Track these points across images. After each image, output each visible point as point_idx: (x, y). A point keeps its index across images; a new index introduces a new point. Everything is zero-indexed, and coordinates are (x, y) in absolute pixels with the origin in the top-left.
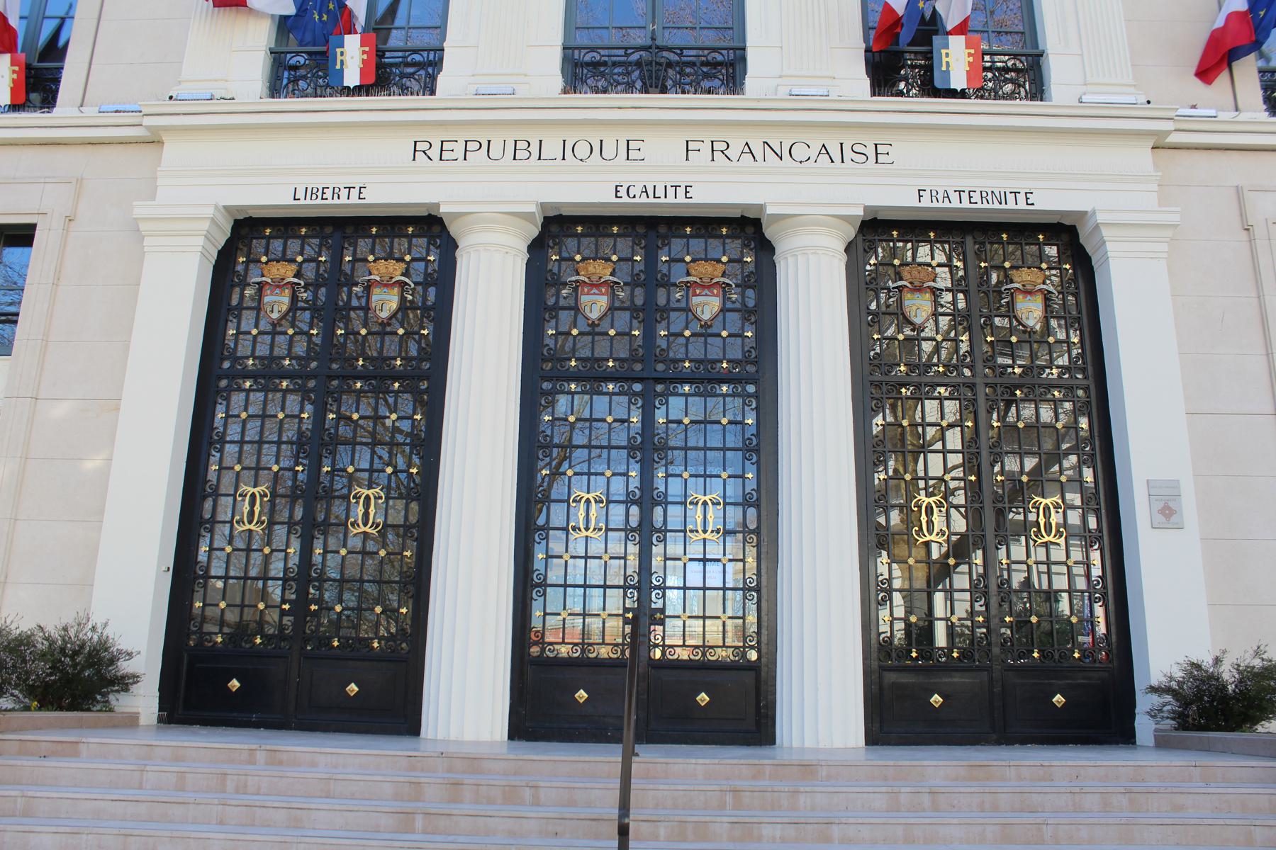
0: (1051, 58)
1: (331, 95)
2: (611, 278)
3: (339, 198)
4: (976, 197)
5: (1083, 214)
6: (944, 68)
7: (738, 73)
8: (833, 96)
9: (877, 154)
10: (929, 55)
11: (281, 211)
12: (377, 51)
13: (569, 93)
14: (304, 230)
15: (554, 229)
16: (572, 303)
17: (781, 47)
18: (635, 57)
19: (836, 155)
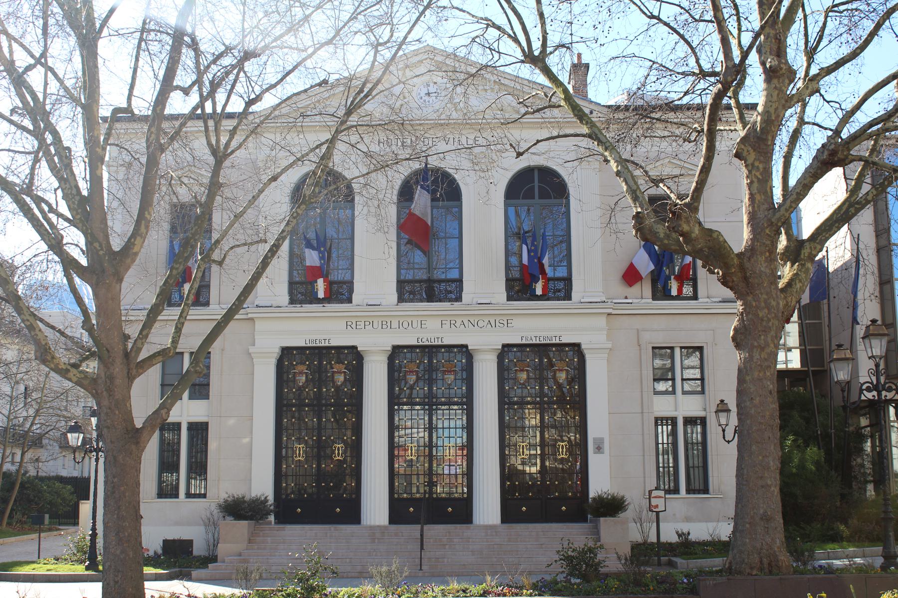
4: (542, 339)
19: (493, 325)
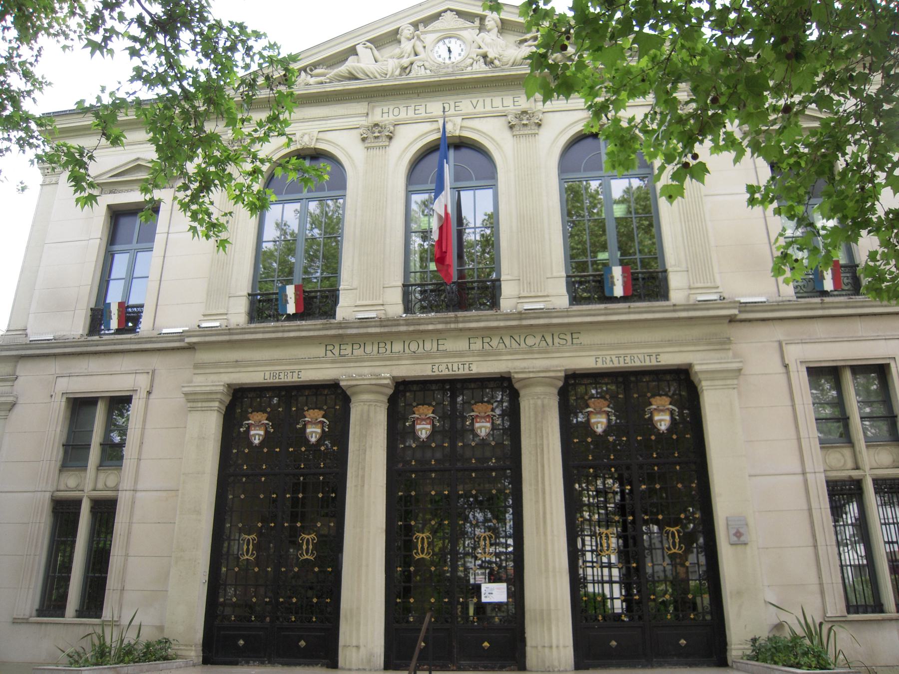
2: (491, 413)
16: (470, 428)
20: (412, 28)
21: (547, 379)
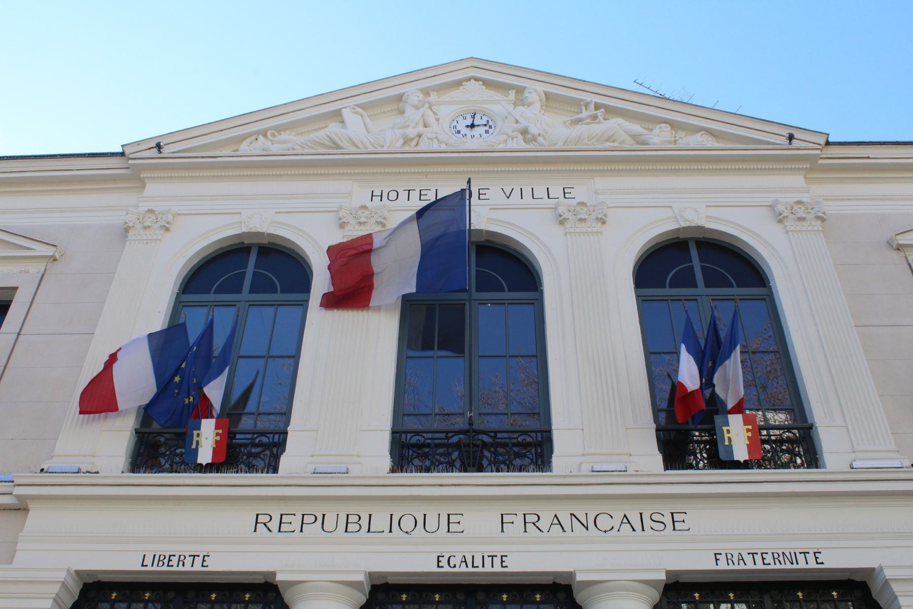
0: (819, 429)
1: (185, 471)
3: (183, 565)
4: (769, 559)
5: (872, 570)
6: (727, 443)
7: (545, 452)
8: (631, 471)
9: (674, 522)
10: (712, 432)
11: (128, 576)
12: (229, 433)
13: (396, 472)
14: (148, 595)
15: (381, 596)
17: (583, 429)
18: (455, 439)
19: (637, 524)
20: (421, 96)
21: (630, 582)
